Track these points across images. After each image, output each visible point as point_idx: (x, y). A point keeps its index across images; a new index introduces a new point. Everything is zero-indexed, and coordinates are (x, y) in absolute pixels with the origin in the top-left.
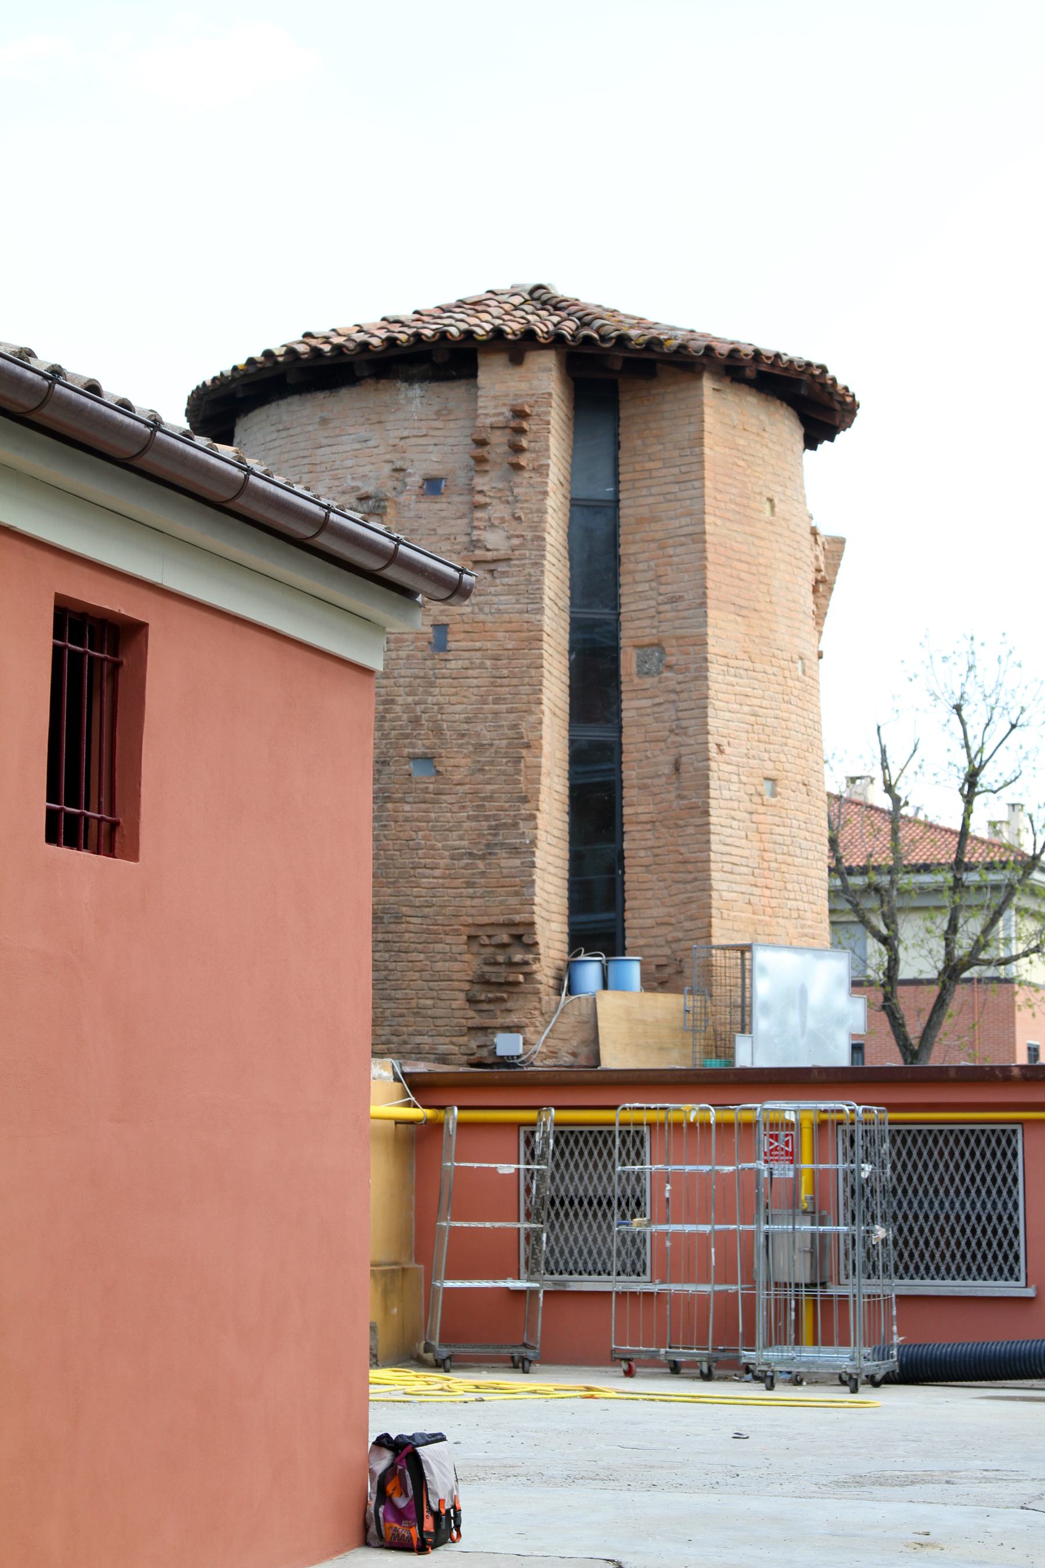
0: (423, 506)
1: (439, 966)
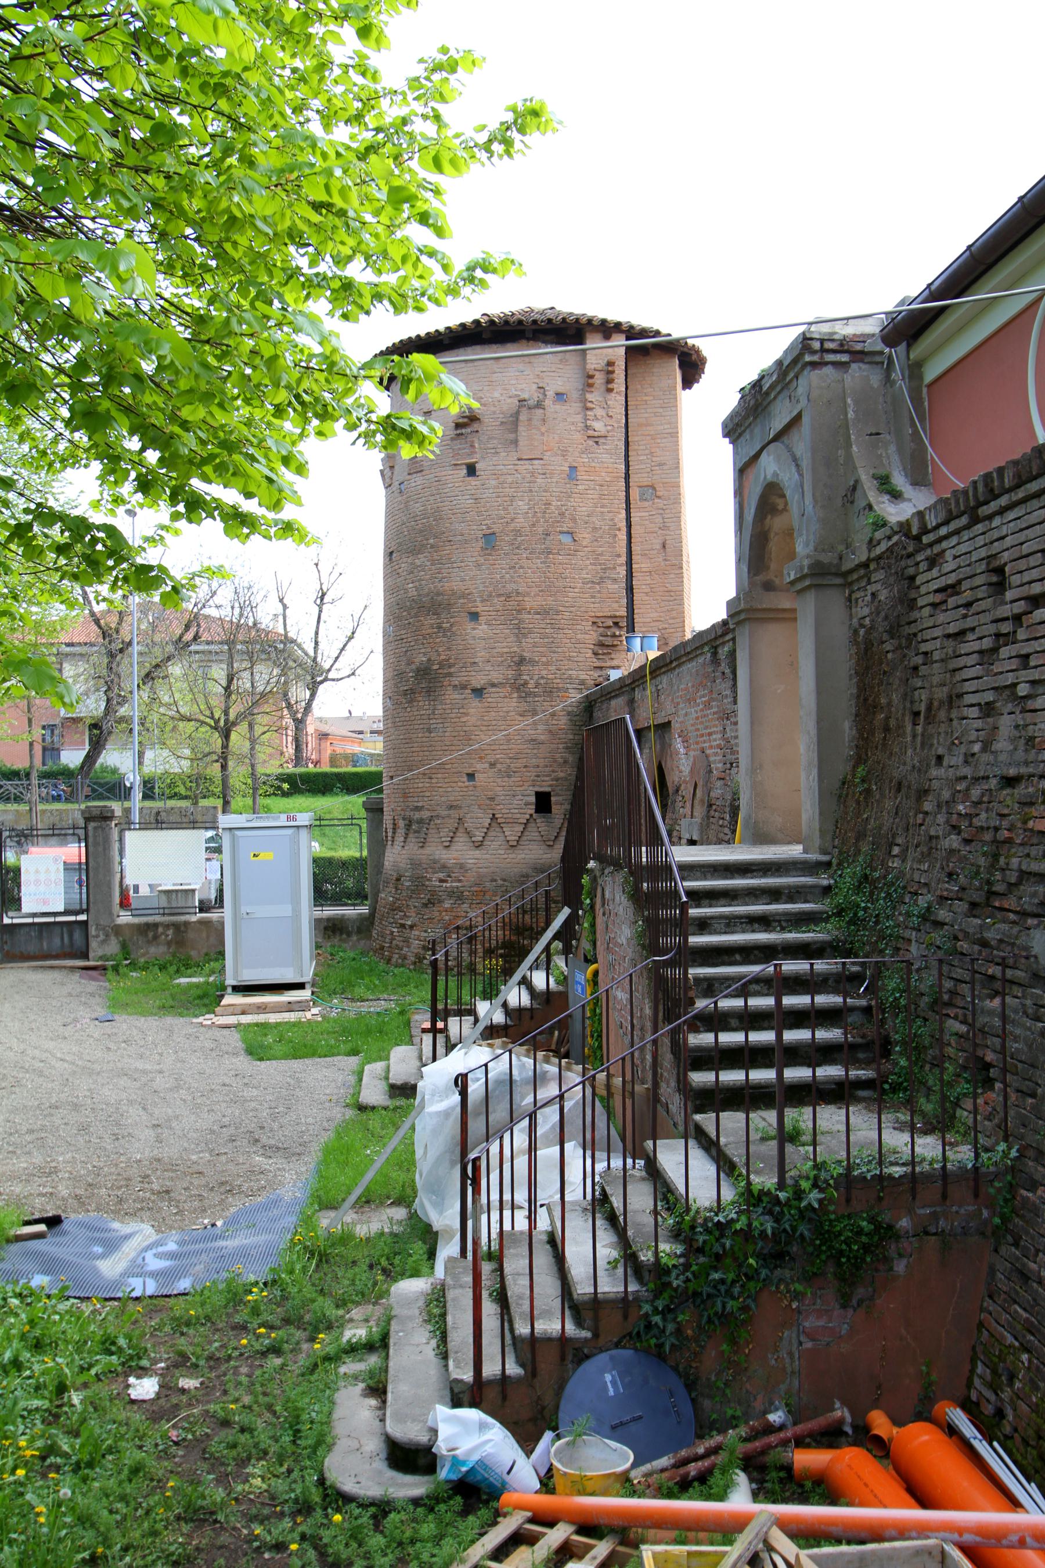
0: (558, 407)
1: (579, 636)
